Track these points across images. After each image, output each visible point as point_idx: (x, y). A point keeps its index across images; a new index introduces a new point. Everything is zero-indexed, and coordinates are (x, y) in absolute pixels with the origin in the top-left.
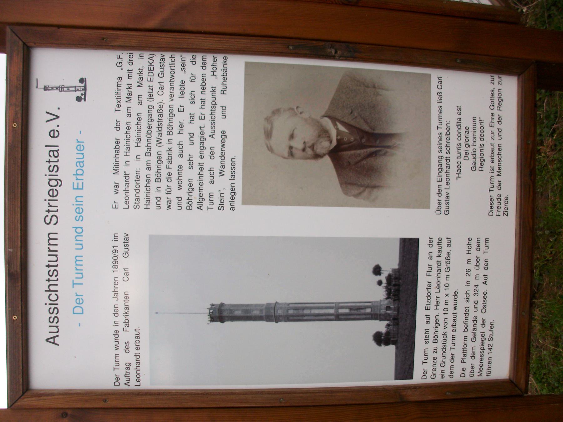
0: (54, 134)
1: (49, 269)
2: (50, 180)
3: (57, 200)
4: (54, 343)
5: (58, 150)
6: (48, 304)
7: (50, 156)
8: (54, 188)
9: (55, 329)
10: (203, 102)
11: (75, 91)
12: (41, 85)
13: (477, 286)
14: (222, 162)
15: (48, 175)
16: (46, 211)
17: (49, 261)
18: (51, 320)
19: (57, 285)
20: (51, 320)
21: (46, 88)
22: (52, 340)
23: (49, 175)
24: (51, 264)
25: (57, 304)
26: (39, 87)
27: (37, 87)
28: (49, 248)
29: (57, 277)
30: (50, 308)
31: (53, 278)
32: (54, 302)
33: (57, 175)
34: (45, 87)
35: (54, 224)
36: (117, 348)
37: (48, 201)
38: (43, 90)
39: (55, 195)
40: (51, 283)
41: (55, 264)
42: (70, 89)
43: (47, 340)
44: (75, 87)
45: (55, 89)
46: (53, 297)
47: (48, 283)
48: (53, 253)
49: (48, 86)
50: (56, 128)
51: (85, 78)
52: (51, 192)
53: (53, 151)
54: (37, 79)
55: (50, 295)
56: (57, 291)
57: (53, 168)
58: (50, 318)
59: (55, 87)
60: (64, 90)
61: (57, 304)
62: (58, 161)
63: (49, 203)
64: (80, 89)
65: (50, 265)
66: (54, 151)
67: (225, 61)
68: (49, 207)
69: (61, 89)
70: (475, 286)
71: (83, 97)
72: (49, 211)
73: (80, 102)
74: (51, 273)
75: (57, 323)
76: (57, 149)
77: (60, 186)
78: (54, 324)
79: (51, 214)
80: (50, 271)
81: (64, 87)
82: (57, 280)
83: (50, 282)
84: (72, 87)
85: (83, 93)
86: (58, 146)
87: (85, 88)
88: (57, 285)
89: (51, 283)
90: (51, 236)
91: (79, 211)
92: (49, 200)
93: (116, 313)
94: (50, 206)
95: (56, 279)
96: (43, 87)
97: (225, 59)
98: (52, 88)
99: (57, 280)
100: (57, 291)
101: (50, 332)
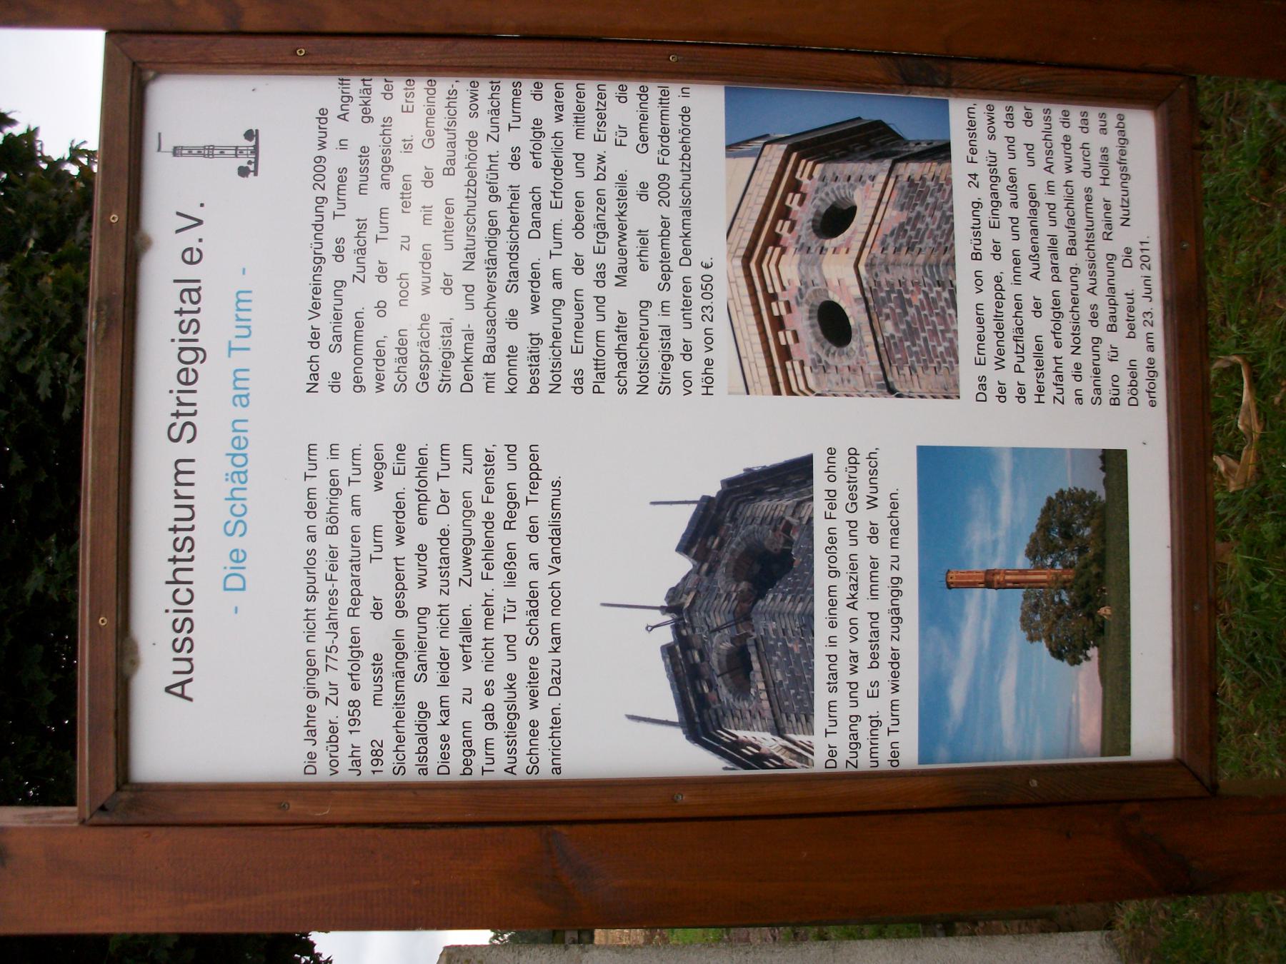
0: (191, 257)
1: (181, 319)
2: (182, 349)
3: (194, 392)
4: (182, 696)
5: (200, 288)
6: (177, 340)
7: (183, 301)
8: (190, 367)
9: (185, 666)
10: (470, 289)
11: (236, 156)
12: (168, 145)
13: (975, 175)
14: (513, 265)
15: (177, 340)
16: (173, 415)
17: (176, 519)
18: (178, 646)
19: (191, 569)
20: (178, 646)
21: (176, 151)
22: (178, 690)
23: (181, 340)
24: (180, 525)
25: (190, 611)
26: (162, 150)
27: (159, 150)
28: (176, 491)
29: (192, 553)
30: (176, 621)
31: (184, 554)
32: (184, 607)
33: (196, 340)
34: (175, 148)
35: (189, 441)
36: (322, 145)
37: (175, 394)
38: (171, 155)
39: (191, 380)
40: (179, 565)
41: (188, 525)
42: (226, 152)
43: (168, 689)
44: (237, 147)
45: (195, 152)
46: (183, 596)
47: (173, 567)
48: (184, 501)
49: (182, 148)
50: (196, 245)
51: (257, 131)
52: (183, 375)
53: (189, 291)
54: (160, 134)
55: (177, 591)
56: (191, 583)
57: (189, 324)
58: (176, 640)
59: (195, 148)
60: (213, 154)
61: (190, 611)
62: (198, 311)
63: (178, 398)
64: (245, 152)
65: (178, 527)
66: (191, 291)
67: (511, 683)
68: (178, 405)
69: (208, 152)
70: (970, 175)
71: (252, 167)
72: (177, 415)
73: (246, 178)
74: (179, 545)
75: (189, 651)
76: (197, 287)
77: (202, 362)
78: (183, 654)
79: (183, 420)
80: (183, 322)
81: (213, 149)
82: (192, 559)
83: (177, 563)
84: (229, 148)
85: (253, 160)
86: (198, 281)
87: (256, 150)
88: (191, 569)
89: (179, 565)
90: (182, 466)
91: (239, 477)
92: (179, 392)
93: (311, 510)
94: (181, 404)
95: (189, 556)
96: (171, 149)
97: (512, 680)
98: (190, 152)
99: (192, 559)
100: (191, 583)
101: (175, 673)
